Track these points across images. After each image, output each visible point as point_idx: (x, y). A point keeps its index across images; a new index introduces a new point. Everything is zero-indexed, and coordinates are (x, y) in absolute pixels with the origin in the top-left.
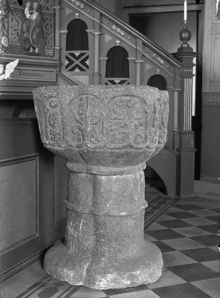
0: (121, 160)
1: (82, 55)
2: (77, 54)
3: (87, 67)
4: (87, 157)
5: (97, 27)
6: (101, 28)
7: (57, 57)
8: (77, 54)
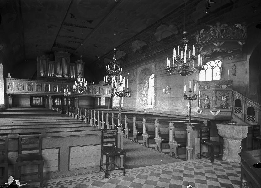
0: (233, 139)
1: (239, 109)
2: (238, 108)
3: (241, 112)
4: (226, 137)
5: (244, 102)
6: (245, 102)
7: (232, 109)
8: (238, 108)
